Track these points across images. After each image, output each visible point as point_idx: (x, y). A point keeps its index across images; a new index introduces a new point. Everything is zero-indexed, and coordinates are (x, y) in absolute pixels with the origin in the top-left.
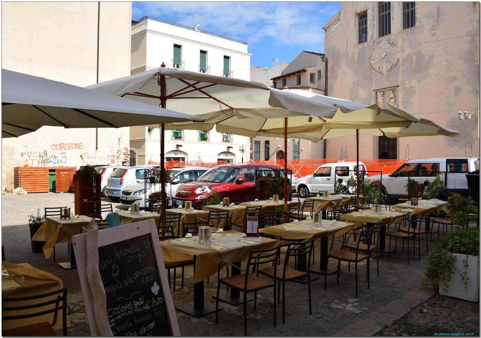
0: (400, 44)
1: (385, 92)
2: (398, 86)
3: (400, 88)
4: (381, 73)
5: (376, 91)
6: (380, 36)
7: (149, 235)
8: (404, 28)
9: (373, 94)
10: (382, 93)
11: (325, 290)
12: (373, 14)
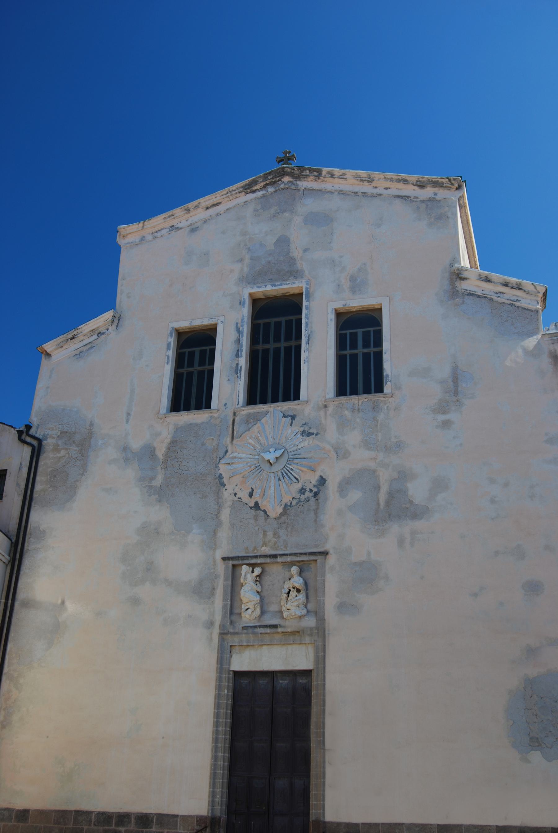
0: (331, 433)
1: (267, 568)
2: (325, 554)
3: (331, 560)
4: (257, 506)
5: (234, 563)
6: (251, 400)
7: (363, 332)
8: (341, 391)
9: (221, 568)
10: (257, 571)
11: (224, 559)
12: (238, 341)
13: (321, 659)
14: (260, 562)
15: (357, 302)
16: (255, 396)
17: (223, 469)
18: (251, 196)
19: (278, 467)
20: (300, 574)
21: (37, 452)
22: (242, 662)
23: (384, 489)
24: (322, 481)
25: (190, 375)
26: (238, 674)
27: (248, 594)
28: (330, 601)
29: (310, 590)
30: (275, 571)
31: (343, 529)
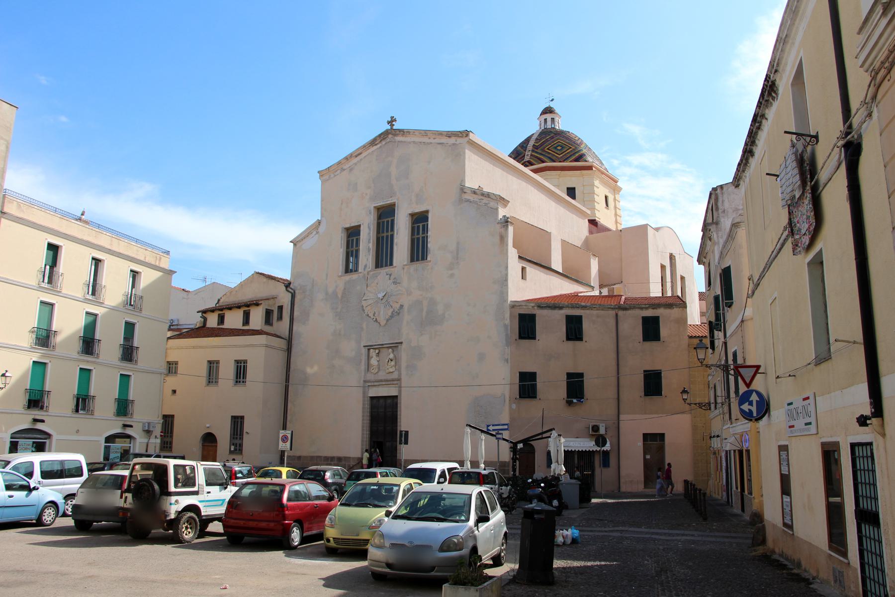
3: (404, 346)
5: (369, 348)
9: (364, 351)
10: (377, 351)
13: (400, 391)
14: (380, 348)
15: (418, 209)
16: (378, 264)
17: (364, 303)
18: (375, 147)
19: (384, 301)
20: (393, 351)
21: (293, 296)
22: (374, 392)
23: (425, 310)
24: (402, 306)
25: (418, 239)
26: (372, 398)
27: (374, 361)
28: (404, 364)
29: (396, 360)
30: (384, 351)
31: (408, 333)
